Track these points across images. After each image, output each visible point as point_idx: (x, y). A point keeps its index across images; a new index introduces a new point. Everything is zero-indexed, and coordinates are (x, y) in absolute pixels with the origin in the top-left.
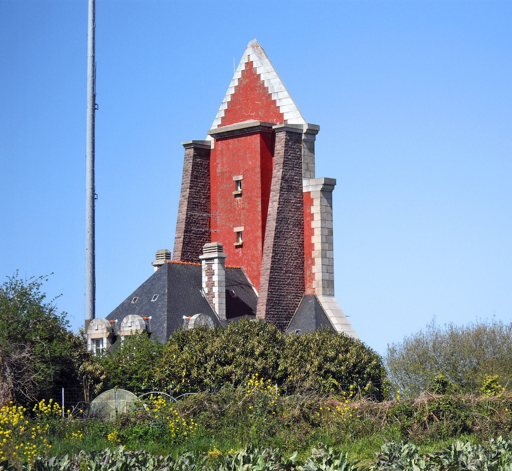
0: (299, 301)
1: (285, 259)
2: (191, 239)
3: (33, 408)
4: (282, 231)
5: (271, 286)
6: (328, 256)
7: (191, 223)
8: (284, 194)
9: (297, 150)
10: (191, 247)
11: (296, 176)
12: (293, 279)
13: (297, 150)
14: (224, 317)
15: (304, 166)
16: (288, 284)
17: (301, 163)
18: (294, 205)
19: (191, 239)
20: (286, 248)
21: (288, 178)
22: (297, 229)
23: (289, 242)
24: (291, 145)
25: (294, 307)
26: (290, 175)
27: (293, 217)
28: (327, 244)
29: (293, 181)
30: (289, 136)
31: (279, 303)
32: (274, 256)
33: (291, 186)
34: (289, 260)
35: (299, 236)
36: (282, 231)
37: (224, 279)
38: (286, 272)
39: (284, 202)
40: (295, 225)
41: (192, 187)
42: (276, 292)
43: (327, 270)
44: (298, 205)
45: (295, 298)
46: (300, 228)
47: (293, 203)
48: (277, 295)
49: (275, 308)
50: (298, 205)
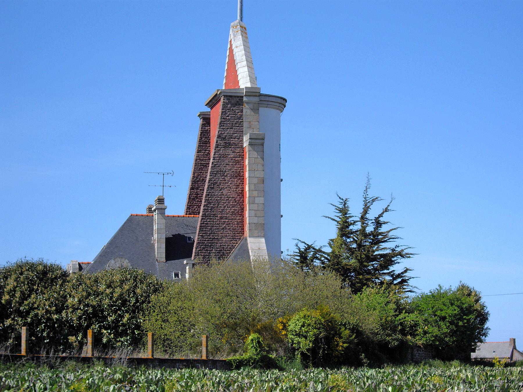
0: (237, 243)
1: (220, 207)
2: (198, 194)
3: (366, 357)
4: (217, 183)
5: (202, 231)
6: (256, 202)
7: (198, 181)
8: (220, 150)
9: (237, 111)
10: (198, 201)
11: (236, 133)
12: (230, 224)
13: (237, 111)
14: (164, 260)
15: (245, 125)
16: (223, 229)
17: (243, 122)
18: (232, 159)
19: (198, 194)
20: (221, 198)
21: (226, 136)
22: (236, 180)
23: (225, 192)
24: (231, 107)
25: (230, 248)
26: (228, 133)
27: (231, 169)
28: (257, 192)
29: (232, 138)
30: (228, 99)
31: (211, 245)
32: (207, 205)
33: (230, 143)
34: (225, 207)
35: (238, 185)
36: (217, 183)
37: (163, 227)
38: (221, 218)
39: (220, 157)
40: (232, 177)
41: (200, 150)
42: (209, 236)
43: (256, 214)
44: (237, 159)
45: (231, 241)
46: (239, 179)
47: (231, 157)
48: (210, 238)
49: (207, 250)
50: (237, 159)
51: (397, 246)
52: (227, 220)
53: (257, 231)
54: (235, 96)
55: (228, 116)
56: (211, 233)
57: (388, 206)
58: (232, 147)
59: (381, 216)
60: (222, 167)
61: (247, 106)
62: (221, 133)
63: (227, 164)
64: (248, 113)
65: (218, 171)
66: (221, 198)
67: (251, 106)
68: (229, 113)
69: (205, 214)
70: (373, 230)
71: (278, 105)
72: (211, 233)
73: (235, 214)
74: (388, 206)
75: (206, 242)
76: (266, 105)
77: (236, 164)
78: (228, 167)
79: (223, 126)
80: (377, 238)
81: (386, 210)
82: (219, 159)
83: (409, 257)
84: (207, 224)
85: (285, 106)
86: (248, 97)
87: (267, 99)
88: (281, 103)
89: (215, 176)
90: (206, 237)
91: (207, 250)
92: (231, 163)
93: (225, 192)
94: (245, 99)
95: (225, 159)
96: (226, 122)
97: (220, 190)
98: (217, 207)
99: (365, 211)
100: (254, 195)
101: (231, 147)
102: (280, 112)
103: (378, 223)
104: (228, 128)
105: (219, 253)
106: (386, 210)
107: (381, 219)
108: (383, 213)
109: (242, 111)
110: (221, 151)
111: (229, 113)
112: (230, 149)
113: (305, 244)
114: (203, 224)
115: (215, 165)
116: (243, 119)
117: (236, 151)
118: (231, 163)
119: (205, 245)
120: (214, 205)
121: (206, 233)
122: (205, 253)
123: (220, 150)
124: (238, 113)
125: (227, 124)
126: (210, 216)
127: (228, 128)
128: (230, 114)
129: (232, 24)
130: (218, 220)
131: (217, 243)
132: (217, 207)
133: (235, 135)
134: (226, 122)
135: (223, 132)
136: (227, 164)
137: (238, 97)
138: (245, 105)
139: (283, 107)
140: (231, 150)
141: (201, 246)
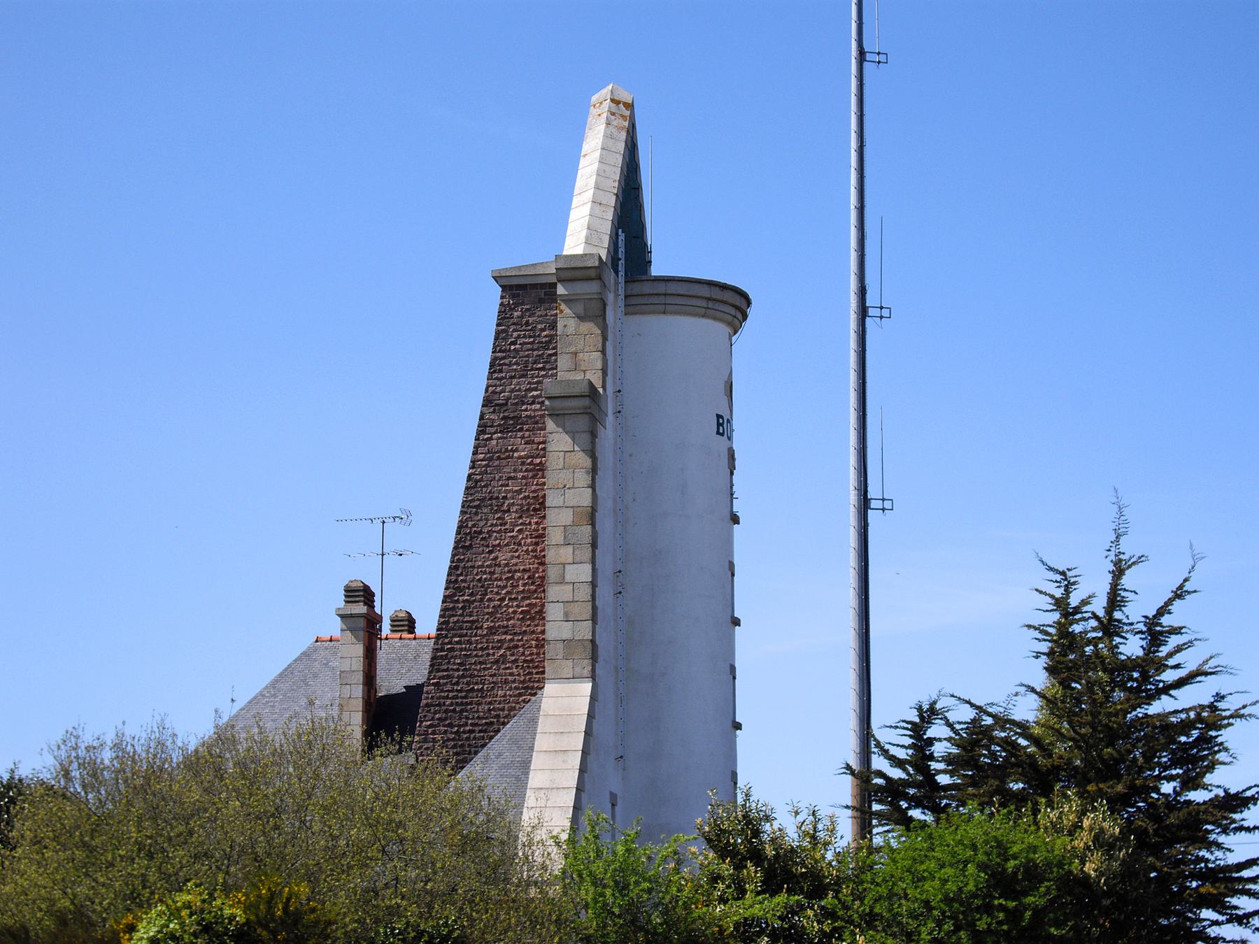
1: (490, 600)
4: (481, 532)
6: (568, 578)
9: (539, 326)
11: (536, 389)
12: (517, 647)
13: (539, 326)
16: (497, 662)
18: (523, 464)
20: (492, 573)
21: (508, 399)
23: (503, 557)
24: (522, 317)
26: (512, 391)
27: (520, 492)
28: (570, 549)
30: (513, 296)
31: (462, 711)
32: (454, 595)
34: (502, 600)
36: (481, 532)
39: (491, 459)
42: (457, 683)
43: (566, 614)
45: (520, 695)
47: (520, 457)
49: (450, 725)
51: (1220, 697)
52: (509, 637)
53: (570, 663)
54: (534, 286)
55: (513, 343)
56: (463, 676)
57: (1186, 580)
58: (526, 427)
59: (1162, 611)
60: (496, 488)
61: (567, 311)
62: (494, 392)
63: (509, 478)
64: (571, 330)
65: (482, 500)
66: (492, 573)
67: (580, 308)
68: (515, 334)
69: (447, 623)
70: (1140, 653)
71: (704, 304)
72: (463, 676)
73: (532, 619)
74: (1186, 580)
75: (448, 702)
76: (661, 308)
77: (534, 477)
78: (513, 487)
79: (501, 371)
80: (1145, 676)
81: (1179, 594)
82: (487, 466)
83: (1230, 724)
84: (452, 650)
85: (745, 317)
86: (569, 284)
87: (672, 288)
88: (730, 304)
89: (476, 514)
90: (449, 687)
91: (450, 725)
92: (520, 475)
93: (503, 557)
94: (561, 290)
95: (504, 462)
96: (507, 361)
97: (490, 552)
98: (482, 600)
99: (1115, 600)
100: (562, 560)
101: (521, 430)
102: (722, 329)
103: (1155, 633)
104: (512, 377)
105: (485, 731)
106: (1179, 594)
107: (1166, 620)
108: (1169, 602)
109: (553, 326)
110: (494, 442)
111: (515, 334)
112: (520, 434)
113: (972, 705)
114: (442, 650)
115: (477, 481)
116: (555, 348)
117: (536, 440)
118: (520, 475)
119: (446, 711)
120: (471, 595)
121: (448, 677)
122: (445, 732)
123: (491, 439)
124: (543, 330)
125: (510, 365)
126: (461, 628)
127: (512, 377)
128: (519, 336)
129: (594, 98)
130: (483, 636)
131: (479, 704)
132: (482, 600)
133: (535, 393)
134: (507, 361)
135: (499, 389)
136: (509, 478)
137: (543, 286)
138: (563, 306)
139: (740, 316)
140: (522, 437)
141: (435, 713)
